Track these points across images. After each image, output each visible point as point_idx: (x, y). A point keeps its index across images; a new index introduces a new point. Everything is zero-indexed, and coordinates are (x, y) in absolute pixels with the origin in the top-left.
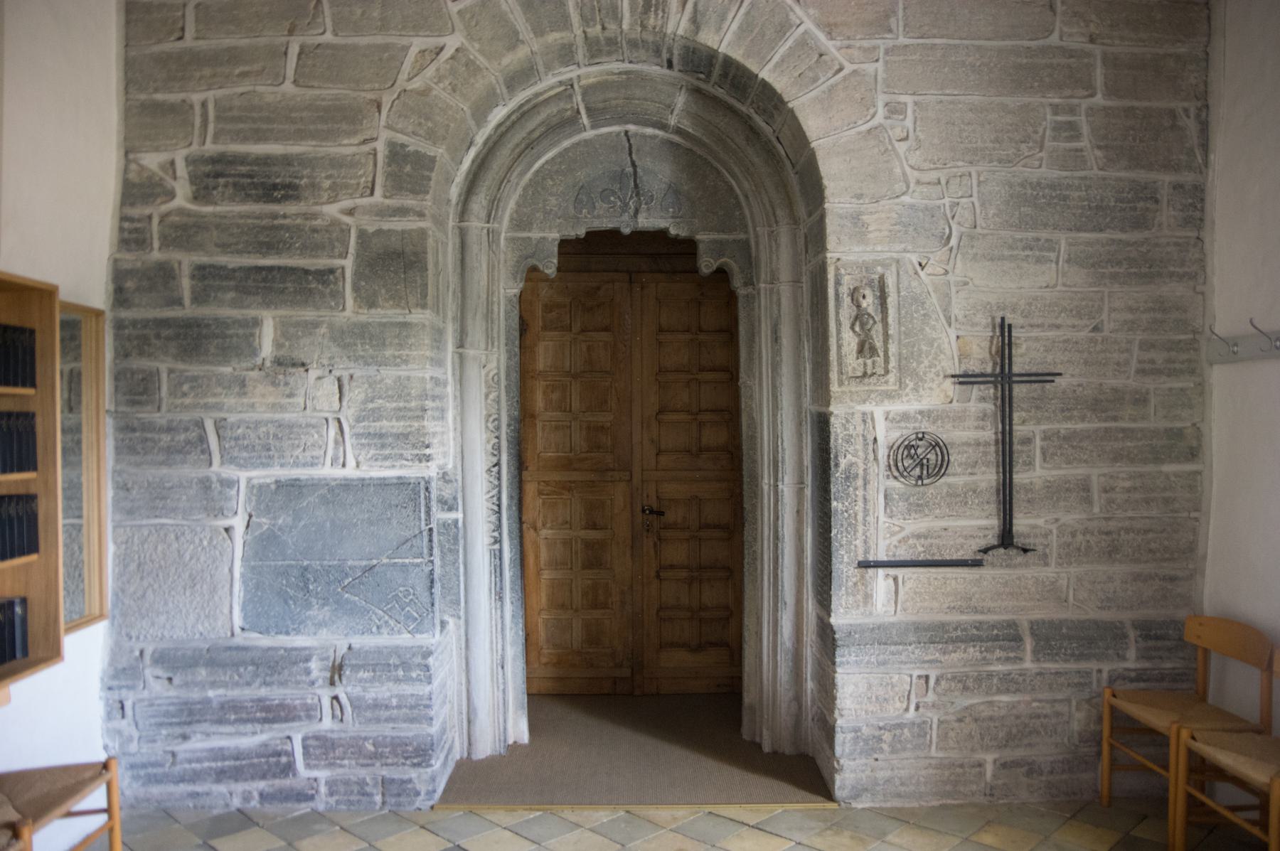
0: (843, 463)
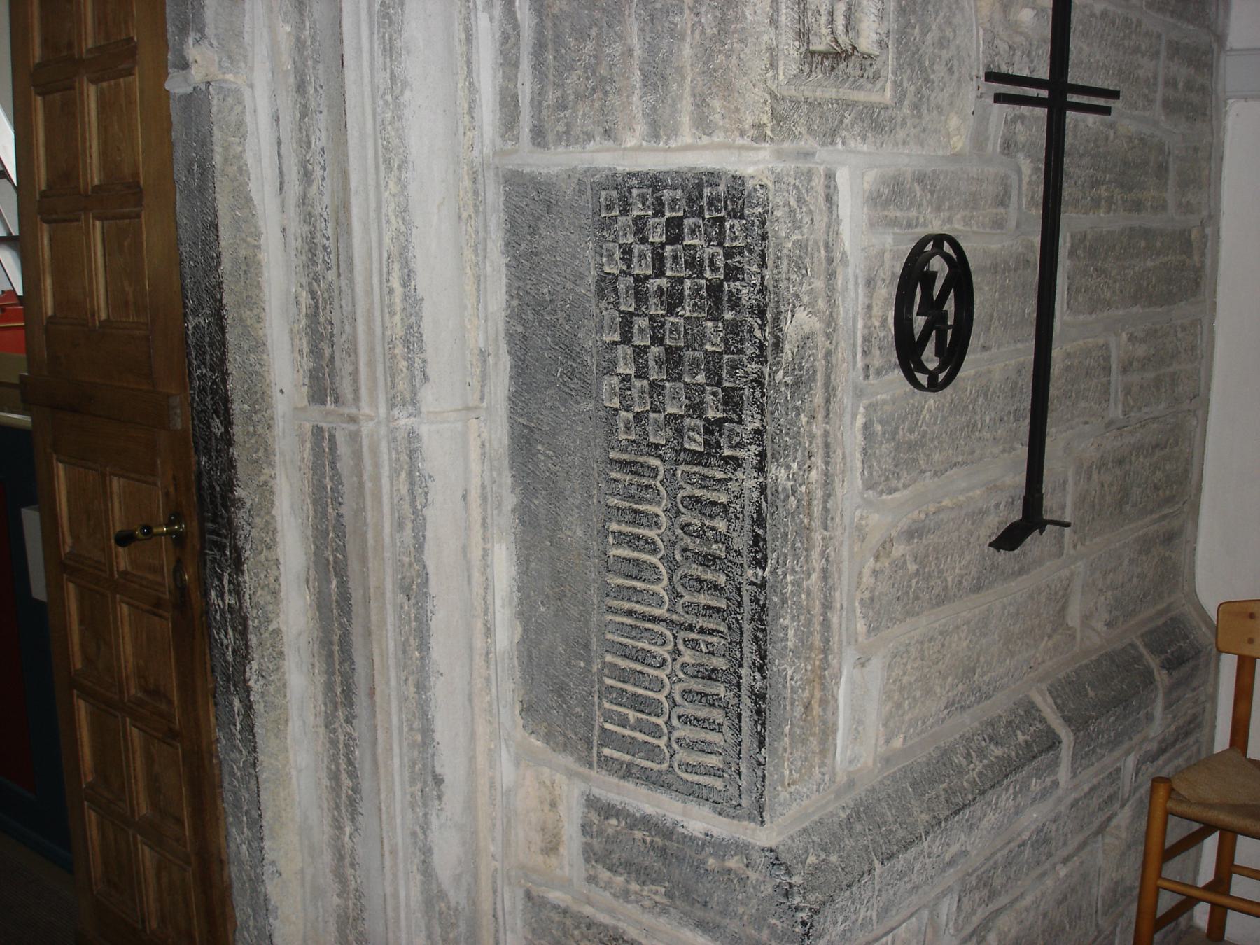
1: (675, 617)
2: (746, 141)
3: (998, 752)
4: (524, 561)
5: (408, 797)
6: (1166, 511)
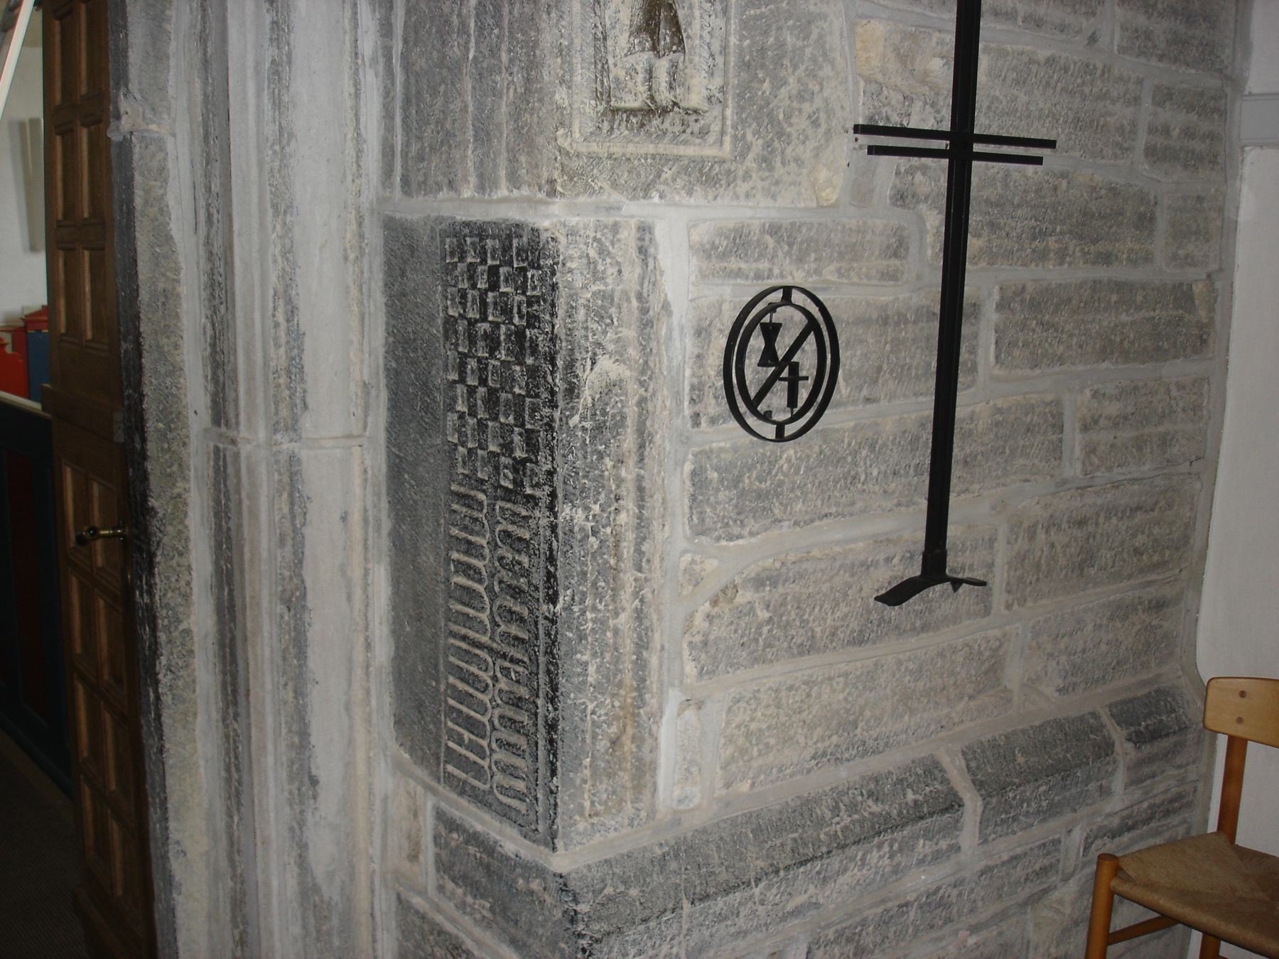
0: (590, 381)
1: (495, 645)
2: (541, 195)
3: (876, 808)
4: (396, 582)
5: (286, 794)
6: (1153, 577)
